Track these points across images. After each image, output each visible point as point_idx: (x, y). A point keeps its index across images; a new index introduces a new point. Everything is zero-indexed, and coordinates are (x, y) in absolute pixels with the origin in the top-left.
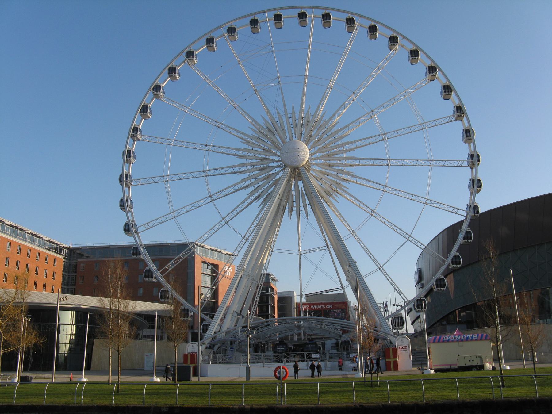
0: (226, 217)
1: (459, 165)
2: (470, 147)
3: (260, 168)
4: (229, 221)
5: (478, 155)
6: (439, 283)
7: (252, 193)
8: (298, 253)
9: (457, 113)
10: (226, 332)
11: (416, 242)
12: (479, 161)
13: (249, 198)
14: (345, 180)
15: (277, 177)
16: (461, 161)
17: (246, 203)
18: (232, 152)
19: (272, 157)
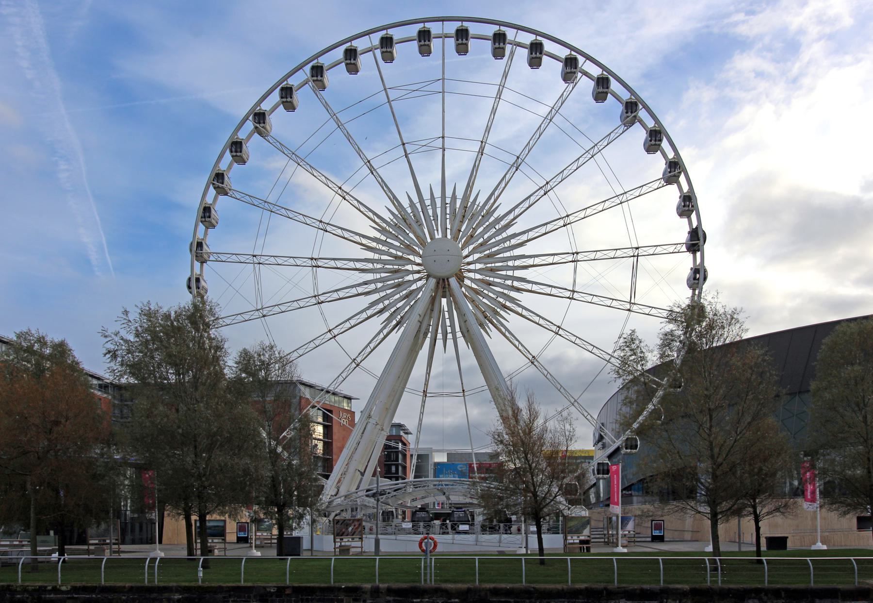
0: (333, 329)
3: (392, 270)
4: (338, 335)
5: (705, 271)
6: (601, 468)
7: (389, 320)
10: (346, 496)
13: (384, 327)
14: (505, 307)
17: (364, 316)
18: (357, 238)
19: (411, 257)
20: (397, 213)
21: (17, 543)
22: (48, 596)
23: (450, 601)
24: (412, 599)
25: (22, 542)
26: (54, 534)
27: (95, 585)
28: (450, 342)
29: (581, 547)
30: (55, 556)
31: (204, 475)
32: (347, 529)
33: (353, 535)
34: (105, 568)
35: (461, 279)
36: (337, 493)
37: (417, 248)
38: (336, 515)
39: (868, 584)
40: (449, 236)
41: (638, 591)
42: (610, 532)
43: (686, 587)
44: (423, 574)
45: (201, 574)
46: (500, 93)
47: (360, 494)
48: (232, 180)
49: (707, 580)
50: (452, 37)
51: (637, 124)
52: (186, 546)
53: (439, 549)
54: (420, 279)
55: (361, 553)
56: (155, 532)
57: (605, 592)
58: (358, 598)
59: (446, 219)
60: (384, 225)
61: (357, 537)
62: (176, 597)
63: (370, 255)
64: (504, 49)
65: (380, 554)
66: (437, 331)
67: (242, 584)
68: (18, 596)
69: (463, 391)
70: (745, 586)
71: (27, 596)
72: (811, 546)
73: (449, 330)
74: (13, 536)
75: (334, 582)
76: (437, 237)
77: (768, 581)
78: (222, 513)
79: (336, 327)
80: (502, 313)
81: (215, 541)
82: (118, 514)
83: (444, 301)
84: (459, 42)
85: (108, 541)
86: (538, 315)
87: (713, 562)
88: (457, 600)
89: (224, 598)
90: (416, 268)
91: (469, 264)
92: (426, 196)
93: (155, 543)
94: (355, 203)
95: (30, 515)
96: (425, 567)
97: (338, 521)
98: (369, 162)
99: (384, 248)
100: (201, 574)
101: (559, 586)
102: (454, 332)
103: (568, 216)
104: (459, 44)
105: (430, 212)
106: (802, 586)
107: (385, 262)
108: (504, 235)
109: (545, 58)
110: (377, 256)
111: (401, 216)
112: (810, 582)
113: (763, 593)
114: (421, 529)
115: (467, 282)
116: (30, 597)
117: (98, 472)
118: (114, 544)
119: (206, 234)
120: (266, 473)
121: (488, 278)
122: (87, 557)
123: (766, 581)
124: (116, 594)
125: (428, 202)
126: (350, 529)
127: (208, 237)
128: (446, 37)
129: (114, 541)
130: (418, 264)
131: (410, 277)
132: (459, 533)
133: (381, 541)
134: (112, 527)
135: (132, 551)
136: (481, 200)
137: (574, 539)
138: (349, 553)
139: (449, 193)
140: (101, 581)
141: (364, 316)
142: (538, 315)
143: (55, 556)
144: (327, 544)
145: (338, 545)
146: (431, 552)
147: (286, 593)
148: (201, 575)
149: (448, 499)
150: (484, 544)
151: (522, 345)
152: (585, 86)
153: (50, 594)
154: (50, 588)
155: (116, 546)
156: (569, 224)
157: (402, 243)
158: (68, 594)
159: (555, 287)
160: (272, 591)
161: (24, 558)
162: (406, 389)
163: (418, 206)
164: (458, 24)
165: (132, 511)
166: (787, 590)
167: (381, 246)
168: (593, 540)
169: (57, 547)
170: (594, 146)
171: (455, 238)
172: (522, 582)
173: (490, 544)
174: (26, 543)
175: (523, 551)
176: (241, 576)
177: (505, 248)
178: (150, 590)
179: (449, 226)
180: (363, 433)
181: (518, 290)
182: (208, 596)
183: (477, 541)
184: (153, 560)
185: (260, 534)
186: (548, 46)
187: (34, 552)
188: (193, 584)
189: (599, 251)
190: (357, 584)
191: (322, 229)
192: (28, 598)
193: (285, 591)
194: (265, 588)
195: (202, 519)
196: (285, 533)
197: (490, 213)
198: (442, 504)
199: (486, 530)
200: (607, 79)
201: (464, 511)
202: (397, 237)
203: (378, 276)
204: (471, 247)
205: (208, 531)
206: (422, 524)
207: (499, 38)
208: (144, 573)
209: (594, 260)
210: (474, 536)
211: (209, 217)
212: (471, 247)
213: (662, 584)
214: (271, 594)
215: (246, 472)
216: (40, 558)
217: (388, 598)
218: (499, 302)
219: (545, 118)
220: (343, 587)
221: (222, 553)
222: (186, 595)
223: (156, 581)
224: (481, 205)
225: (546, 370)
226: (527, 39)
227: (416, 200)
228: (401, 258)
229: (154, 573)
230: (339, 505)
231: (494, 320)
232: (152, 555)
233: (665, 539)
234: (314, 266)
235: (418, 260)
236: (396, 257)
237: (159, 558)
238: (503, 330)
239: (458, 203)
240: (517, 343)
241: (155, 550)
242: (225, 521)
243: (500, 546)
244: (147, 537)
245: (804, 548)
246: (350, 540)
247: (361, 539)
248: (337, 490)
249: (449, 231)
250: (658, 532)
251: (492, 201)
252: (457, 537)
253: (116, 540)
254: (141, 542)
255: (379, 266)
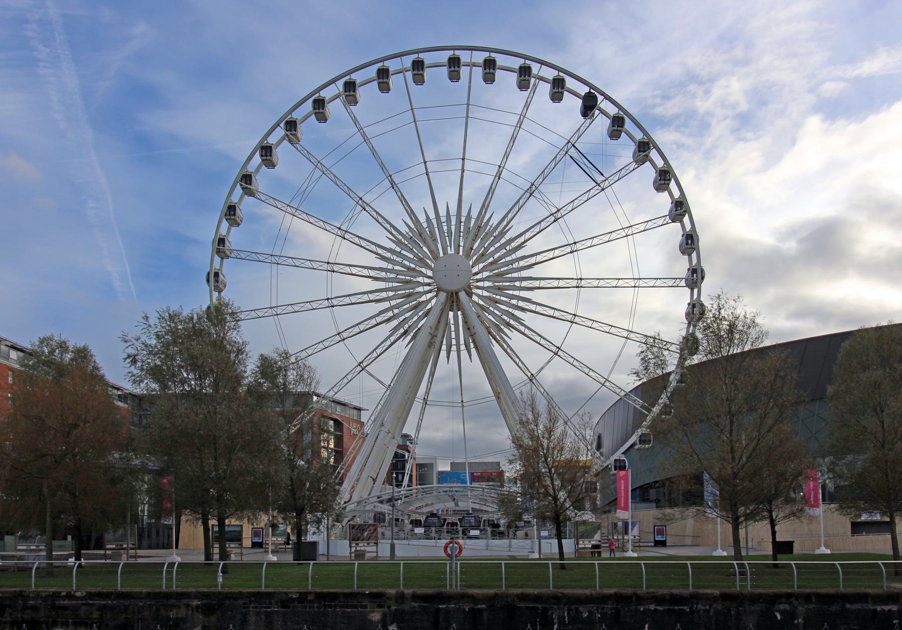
1: (675, 285)
2: (690, 261)
5: (702, 270)
6: (618, 464)
7: (396, 329)
8: (460, 405)
9: (676, 211)
11: (510, 543)
12: (703, 278)
13: (391, 335)
14: (508, 325)
15: (429, 306)
16: (679, 279)
18: (373, 248)
19: (423, 270)
20: (413, 226)
21: (34, 548)
22: (61, 602)
23: (476, 607)
24: (438, 604)
25: (38, 546)
26: (72, 539)
27: (111, 590)
28: (454, 354)
29: (592, 552)
30: (72, 560)
31: (225, 478)
32: (363, 534)
33: (368, 540)
34: (122, 573)
35: (470, 294)
36: (350, 499)
37: (429, 262)
38: (349, 521)
39: (895, 588)
40: (461, 253)
41: (668, 597)
42: (615, 537)
43: (716, 592)
44: (448, 579)
45: (220, 580)
46: (364, 136)
47: (372, 500)
48: (260, 182)
49: (736, 585)
50: (480, 66)
51: (648, 163)
52: (203, 551)
53: (464, 553)
54: (430, 291)
55: (376, 558)
56: (172, 537)
57: (634, 597)
58: (382, 604)
59: (460, 236)
60: (400, 237)
61: (372, 541)
62: (194, 603)
63: (384, 264)
64: (529, 81)
65: (395, 559)
66: (442, 342)
67: (263, 589)
68: (31, 602)
69: (462, 401)
70: (776, 590)
71: (41, 602)
72: (815, 551)
73: (454, 342)
74: (28, 541)
75: (357, 588)
76: (449, 252)
77: (797, 585)
78: (240, 518)
79: (345, 330)
80: (506, 330)
81: (232, 546)
82: (136, 519)
83: (451, 314)
84: (486, 71)
85: (125, 546)
86: (539, 335)
87: (741, 566)
88: (483, 606)
89: (244, 604)
90: (427, 280)
91: (478, 281)
92: (442, 212)
93: (172, 548)
94: (374, 214)
95: (46, 519)
96: (451, 572)
97: (353, 527)
98: (390, 176)
99: (398, 259)
100: (220, 580)
101: (587, 592)
102: (458, 345)
103: (575, 243)
104: (486, 73)
105: (445, 228)
106: (831, 590)
107: (398, 273)
108: (514, 256)
109: (565, 93)
110: (390, 266)
111: (417, 229)
112: (839, 586)
113: (794, 598)
114: (433, 535)
115: (475, 298)
116: (44, 603)
117: (117, 475)
118: (131, 549)
119: (229, 231)
120: (284, 476)
121: (494, 296)
122: (103, 561)
123: (796, 586)
124: (132, 600)
125: (443, 219)
126: (366, 534)
127: (231, 234)
128: (406, 71)
129: (131, 546)
130: (429, 277)
131: (420, 289)
132: (470, 538)
133: (396, 546)
134: (129, 532)
135: (149, 556)
136: (494, 221)
137: (586, 544)
138: (364, 558)
139: (464, 213)
140: (117, 587)
141: (373, 322)
142: (539, 335)
143: (72, 560)
144: (342, 549)
145: (353, 549)
146: (456, 556)
147: (309, 598)
148: (221, 580)
149: (457, 505)
150: (494, 548)
151: (522, 363)
152: (601, 124)
153: (64, 600)
154: (63, 594)
155: (133, 551)
156: (576, 251)
157: (415, 255)
158: (82, 600)
159: (558, 310)
160: (294, 596)
161: (37, 562)
162: (416, 399)
163: (434, 222)
164: (450, 53)
165: (150, 517)
166: (818, 595)
167: (395, 257)
168: (603, 545)
169: (73, 552)
170: (605, 180)
171: (468, 256)
172: (549, 587)
173: (501, 549)
174: (43, 547)
175: (536, 556)
176: (262, 582)
177: (513, 268)
178: (169, 596)
179: (462, 244)
180: (375, 441)
181: (523, 310)
182: (228, 602)
183: (487, 546)
184: (171, 565)
185: (275, 539)
186: (570, 83)
187: (50, 556)
188: (212, 590)
189: (602, 279)
190: (380, 590)
191: (340, 236)
192: (40, 604)
193: (307, 597)
194: (286, 594)
195: (221, 524)
196: (303, 538)
197: (503, 234)
198: (447, 511)
199: (495, 536)
200: (623, 119)
201: (475, 517)
202: (411, 249)
203: (391, 285)
204: (481, 265)
205: (227, 536)
206: (433, 529)
207: (525, 71)
208: (162, 578)
209: (597, 287)
210: (485, 541)
211: (234, 215)
212: (481, 265)
213: (691, 589)
214: (293, 600)
215: (266, 475)
216: (56, 563)
217: (414, 604)
218: (503, 320)
219: (561, 150)
220: (367, 592)
221: (239, 558)
222: (205, 601)
223: (174, 586)
224: (493, 226)
225: (543, 388)
226: (550, 74)
227: (432, 216)
228: (414, 269)
229: (172, 578)
230: (352, 511)
231: (497, 337)
232: (169, 560)
233: (667, 544)
234: (329, 271)
235: (430, 273)
236: (409, 268)
237: (177, 563)
238: (505, 346)
239: (473, 221)
240: (517, 360)
241: (172, 554)
242: (241, 526)
243: (510, 551)
244: (164, 543)
245: (804, 552)
246: (366, 544)
247: (376, 544)
248: (349, 496)
249: (461, 248)
250: (660, 536)
251: (505, 223)
252: (468, 542)
253: (133, 545)
254: (158, 547)
255: (392, 276)
